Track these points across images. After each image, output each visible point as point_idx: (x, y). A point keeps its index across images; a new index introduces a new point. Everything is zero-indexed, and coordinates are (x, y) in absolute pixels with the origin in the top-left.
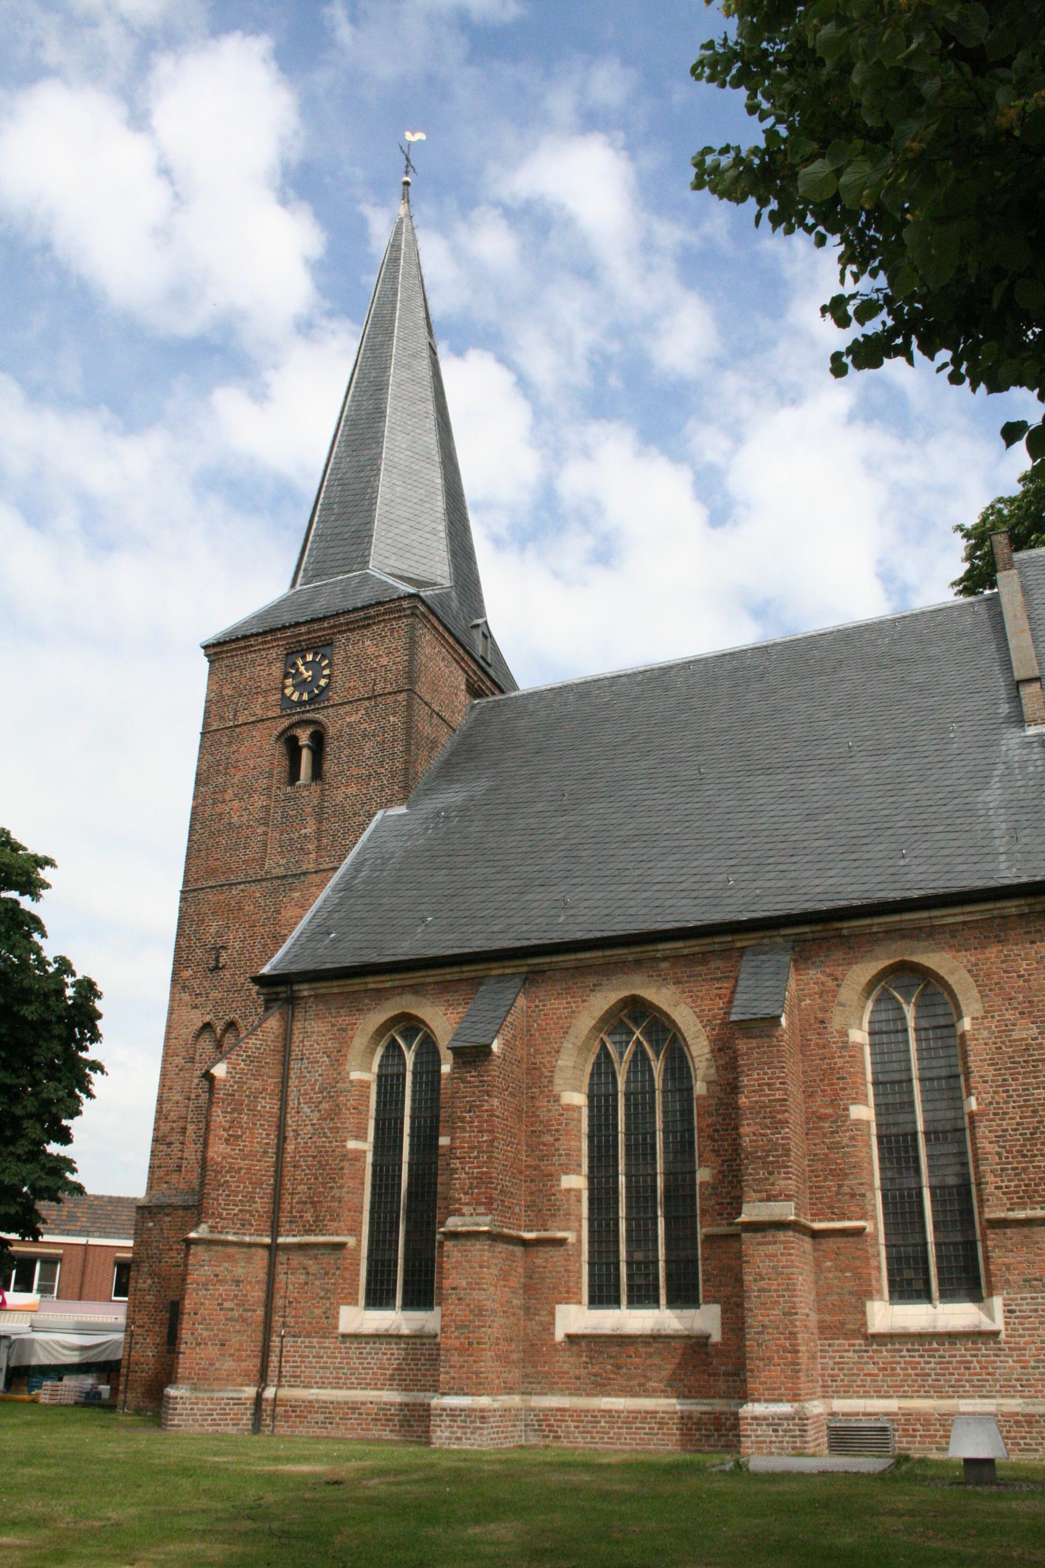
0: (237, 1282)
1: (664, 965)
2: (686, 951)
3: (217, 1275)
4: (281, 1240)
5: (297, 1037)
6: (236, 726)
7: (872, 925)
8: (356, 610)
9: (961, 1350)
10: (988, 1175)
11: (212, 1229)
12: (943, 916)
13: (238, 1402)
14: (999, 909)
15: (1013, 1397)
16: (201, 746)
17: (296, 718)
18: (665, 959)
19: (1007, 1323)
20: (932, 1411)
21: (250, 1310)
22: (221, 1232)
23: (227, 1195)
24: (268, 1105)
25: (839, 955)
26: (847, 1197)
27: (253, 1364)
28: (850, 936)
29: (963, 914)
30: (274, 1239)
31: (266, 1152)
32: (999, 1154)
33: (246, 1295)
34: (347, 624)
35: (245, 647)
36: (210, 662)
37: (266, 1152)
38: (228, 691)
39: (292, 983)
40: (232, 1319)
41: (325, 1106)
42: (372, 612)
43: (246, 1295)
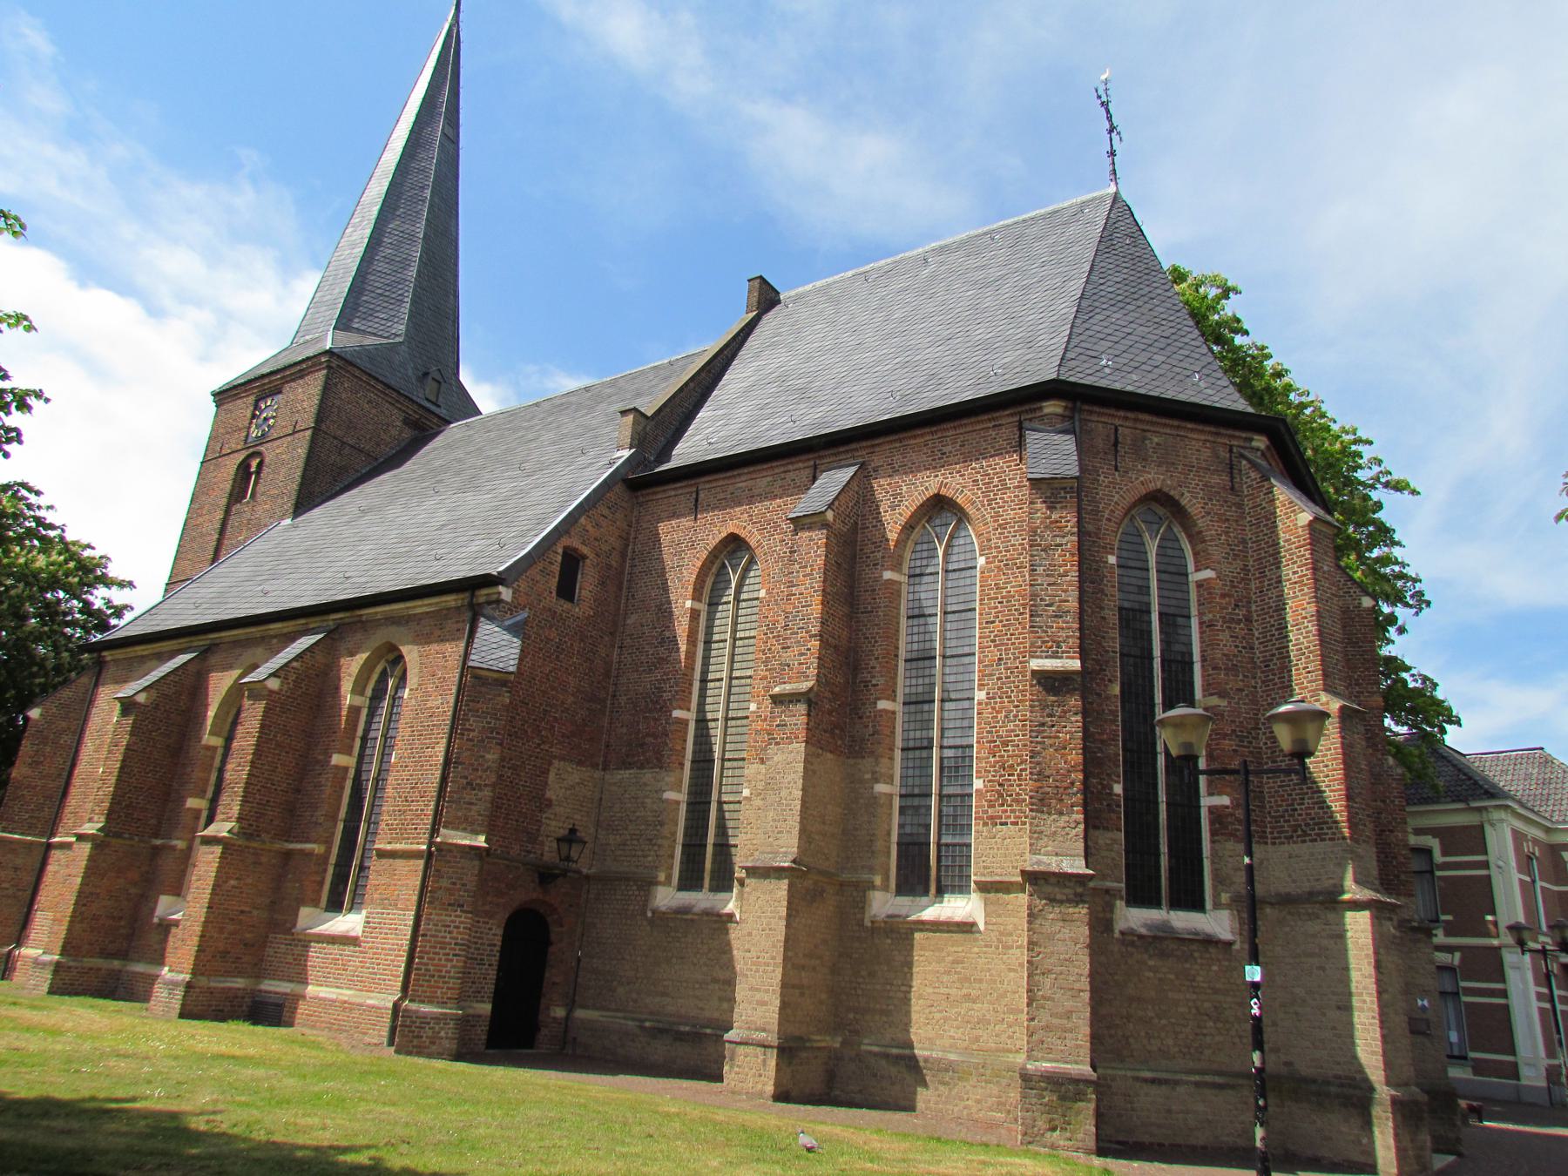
8: (296, 364)
25: (359, 636)
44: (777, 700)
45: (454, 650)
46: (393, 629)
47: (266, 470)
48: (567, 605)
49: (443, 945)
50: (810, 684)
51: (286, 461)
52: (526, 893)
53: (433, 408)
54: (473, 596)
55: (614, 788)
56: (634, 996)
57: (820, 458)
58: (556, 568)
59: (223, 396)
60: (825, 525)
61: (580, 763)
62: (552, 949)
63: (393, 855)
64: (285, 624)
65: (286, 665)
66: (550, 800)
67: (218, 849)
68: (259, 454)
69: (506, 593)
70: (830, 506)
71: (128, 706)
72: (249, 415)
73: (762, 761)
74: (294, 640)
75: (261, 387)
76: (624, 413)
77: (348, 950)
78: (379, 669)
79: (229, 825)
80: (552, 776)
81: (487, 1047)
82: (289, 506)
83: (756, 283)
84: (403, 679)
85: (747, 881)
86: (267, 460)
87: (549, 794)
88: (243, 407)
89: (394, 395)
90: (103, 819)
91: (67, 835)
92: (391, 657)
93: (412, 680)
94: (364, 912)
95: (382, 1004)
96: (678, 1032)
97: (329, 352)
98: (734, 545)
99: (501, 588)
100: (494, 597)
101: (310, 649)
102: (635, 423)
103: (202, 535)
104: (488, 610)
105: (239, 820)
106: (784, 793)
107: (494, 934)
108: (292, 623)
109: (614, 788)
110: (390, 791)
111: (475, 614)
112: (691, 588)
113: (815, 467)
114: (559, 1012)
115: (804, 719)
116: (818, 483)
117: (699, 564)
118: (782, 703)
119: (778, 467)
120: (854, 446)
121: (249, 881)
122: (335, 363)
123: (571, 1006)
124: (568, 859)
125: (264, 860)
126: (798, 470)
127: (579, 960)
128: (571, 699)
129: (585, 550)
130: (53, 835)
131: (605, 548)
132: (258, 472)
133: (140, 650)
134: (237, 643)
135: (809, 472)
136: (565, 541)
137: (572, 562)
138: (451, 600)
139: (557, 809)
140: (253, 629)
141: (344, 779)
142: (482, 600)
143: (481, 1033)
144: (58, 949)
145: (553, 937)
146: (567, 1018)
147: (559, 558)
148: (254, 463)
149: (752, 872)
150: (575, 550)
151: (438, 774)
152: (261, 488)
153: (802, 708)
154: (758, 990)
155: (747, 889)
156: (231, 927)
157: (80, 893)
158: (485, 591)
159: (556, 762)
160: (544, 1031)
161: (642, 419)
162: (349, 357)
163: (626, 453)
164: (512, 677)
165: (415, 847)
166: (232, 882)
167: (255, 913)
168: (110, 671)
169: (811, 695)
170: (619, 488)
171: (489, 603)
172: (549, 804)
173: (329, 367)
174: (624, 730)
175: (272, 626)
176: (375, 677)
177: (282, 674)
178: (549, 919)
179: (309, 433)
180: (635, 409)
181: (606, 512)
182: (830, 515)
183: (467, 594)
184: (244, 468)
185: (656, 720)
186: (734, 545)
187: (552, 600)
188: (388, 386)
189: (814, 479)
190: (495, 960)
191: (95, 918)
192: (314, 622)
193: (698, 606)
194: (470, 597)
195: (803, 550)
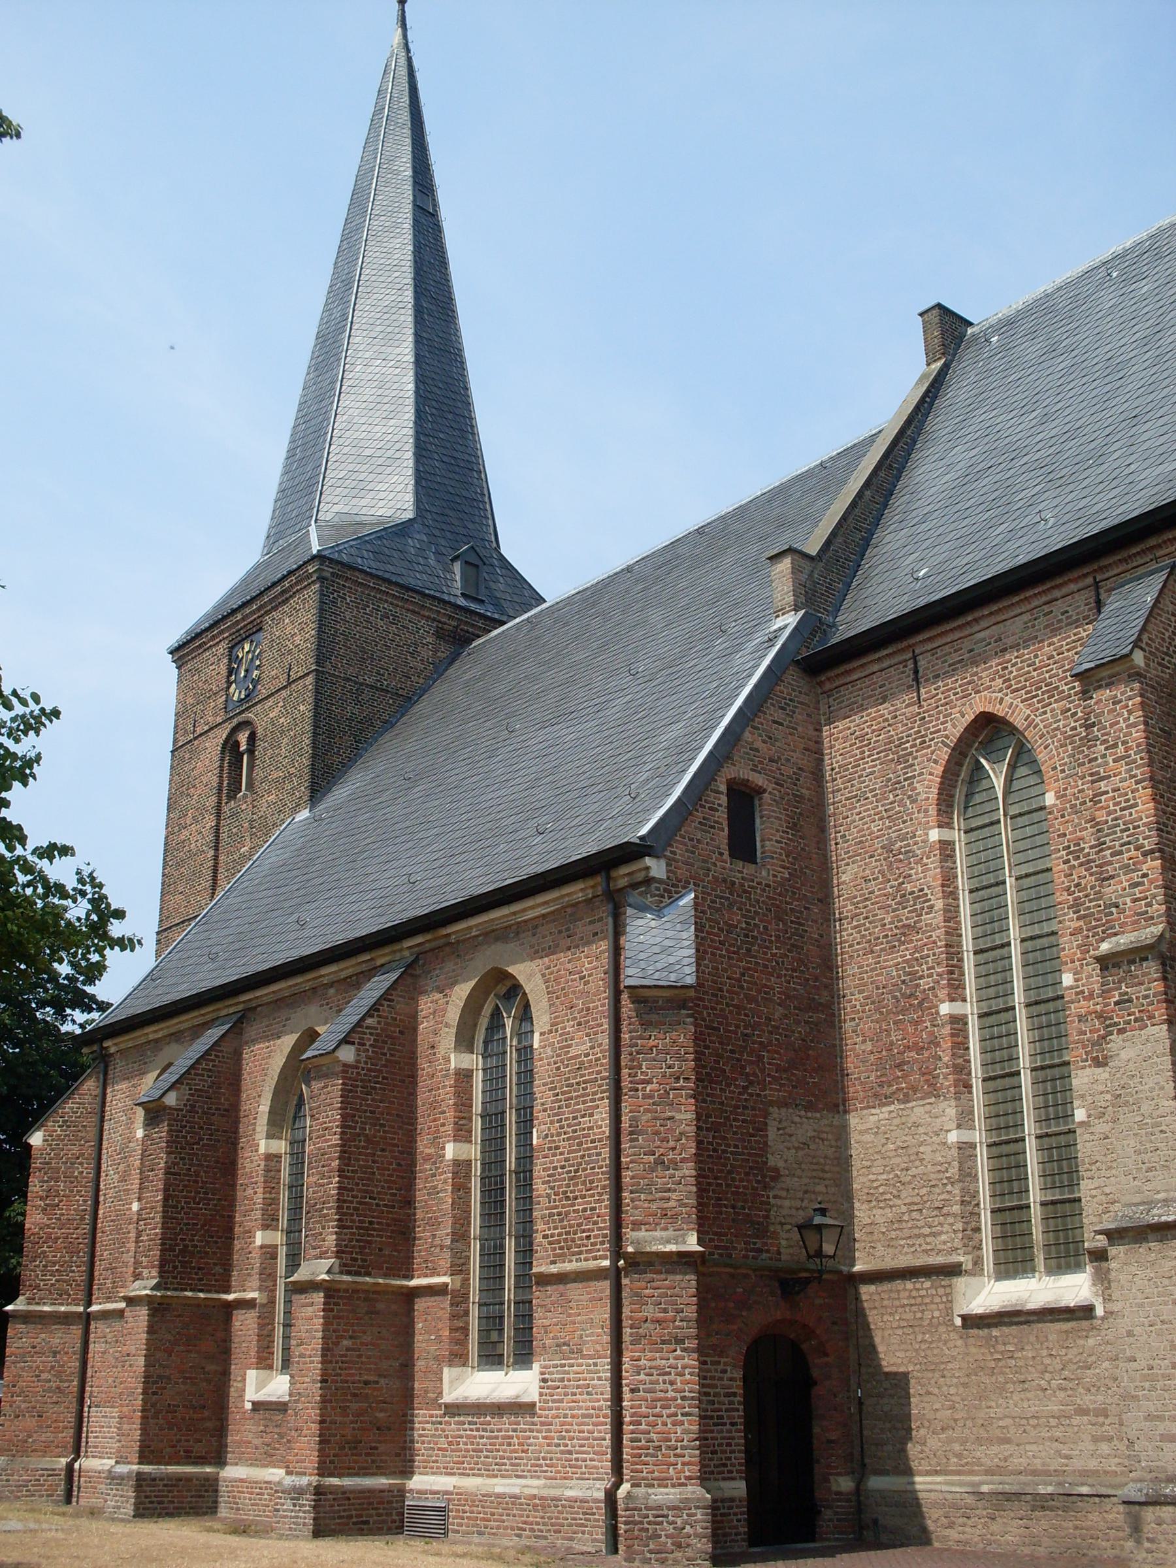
0: (55, 1353)
1: (332, 991)
2: (343, 975)
3: (34, 1347)
4: (94, 1308)
5: (109, 1096)
6: (195, 738)
7: (470, 928)
8: (274, 584)
9: (506, 1423)
10: (539, 1221)
11: (30, 1301)
12: (524, 910)
13: (52, 1472)
14: (567, 895)
15: (538, 1477)
16: (172, 767)
17: (235, 721)
18: (331, 985)
19: (541, 1394)
20: (474, 1490)
21: (67, 1381)
22: (38, 1304)
23: (45, 1266)
24: (85, 1169)
25: (449, 966)
26: (438, 1250)
27: (68, 1435)
28: (458, 942)
29: (539, 905)
30: (86, 1309)
31: (82, 1219)
32: (548, 1196)
33: (63, 1366)
34: (271, 601)
35: (200, 646)
36: (178, 668)
37: (82, 1219)
38: (190, 701)
39: (102, 1040)
40: (50, 1390)
41: (121, 1167)
42: (286, 584)
43: (63, 1366)
44: (1106, 963)
45: (592, 960)
46: (499, 947)
47: (260, 746)
48: (749, 869)
49: (666, 1403)
50: (1157, 929)
51: (285, 722)
52: (768, 1312)
53: (473, 606)
54: (608, 879)
55: (868, 1137)
56: (957, 1447)
57: (1101, 569)
58: (722, 816)
59: (182, 653)
60: (1138, 675)
61: (810, 1107)
62: (816, 1391)
63: (561, 1279)
64: (342, 965)
65: (359, 1024)
66: (776, 1170)
67: (319, 1298)
68: (247, 723)
69: (657, 868)
70: (1136, 644)
71: (154, 1112)
72: (224, 670)
73: (1099, 1063)
74: (358, 986)
75: (231, 628)
76: (775, 558)
77: (523, 1422)
78: (487, 1010)
79: (327, 1263)
80: (772, 1133)
81: (751, 1545)
82: (303, 791)
83: (934, 316)
84: (525, 1015)
85: (1112, 1251)
86: (260, 732)
87: (773, 1161)
88: (214, 663)
89: (417, 599)
90: (154, 1272)
91: (109, 1299)
92: (502, 989)
93: (541, 1019)
94: (536, 1366)
95: (588, 1494)
96: (1036, 1495)
97: (319, 557)
98: (989, 730)
99: (648, 861)
100: (640, 877)
101: (386, 997)
102: (795, 570)
103: (191, 855)
104: (634, 897)
105: (339, 1254)
106: (1146, 1108)
107: (733, 1378)
108: (352, 961)
109: (868, 1137)
110: (540, 1188)
111: (616, 906)
112: (933, 810)
113: (1097, 585)
114: (845, 1484)
115: (1158, 986)
116: (1106, 610)
117: (939, 770)
118: (1117, 965)
119: (1036, 597)
120: (1152, 542)
121: (367, 1338)
122: (328, 571)
123: (861, 1471)
124: (819, 1253)
125: (380, 1306)
126: (1072, 595)
127: (860, 1403)
128: (780, 1011)
129: (759, 780)
130: (89, 1304)
131: (788, 770)
132: (251, 752)
133: (152, 1032)
134: (279, 1003)
135: (1089, 594)
136: (729, 772)
137: (743, 800)
138: (576, 891)
139: (789, 1182)
140: (299, 980)
141: (468, 1176)
142: (622, 883)
143: (739, 1524)
144: (135, 1457)
145: (815, 1373)
146: (858, 1490)
147: (724, 799)
148: (243, 738)
149: (1115, 1235)
150: (745, 783)
151: (606, 1153)
152: (258, 773)
153: (1152, 968)
154: (1160, 1418)
155: (1113, 1265)
156: (354, 1406)
157: (148, 1378)
158: (624, 870)
159: (774, 1110)
160: (827, 1514)
161: (802, 562)
162: (345, 558)
163: (791, 620)
164: (692, 993)
165: (592, 1264)
166: (345, 1343)
167: (383, 1381)
168: (119, 1066)
169: (1164, 947)
170: (793, 677)
171: (634, 886)
172: (776, 1175)
173: (321, 579)
174: (868, 1046)
175: (324, 971)
176: (484, 1022)
177: (356, 1037)
178: (804, 1346)
179: (310, 679)
180: (790, 550)
181: (779, 715)
182: (1139, 658)
183: (599, 879)
184: (230, 746)
185: (916, 1023)
186: (989, 730)
187: (726, 866)
188: (408, 589)
189: (1099, 605)
190: (738, 1415)
191: (171, 1409)
192: (382, 956)
193: (947, 835)
194: (606, 880)
195: (1106, 720)
